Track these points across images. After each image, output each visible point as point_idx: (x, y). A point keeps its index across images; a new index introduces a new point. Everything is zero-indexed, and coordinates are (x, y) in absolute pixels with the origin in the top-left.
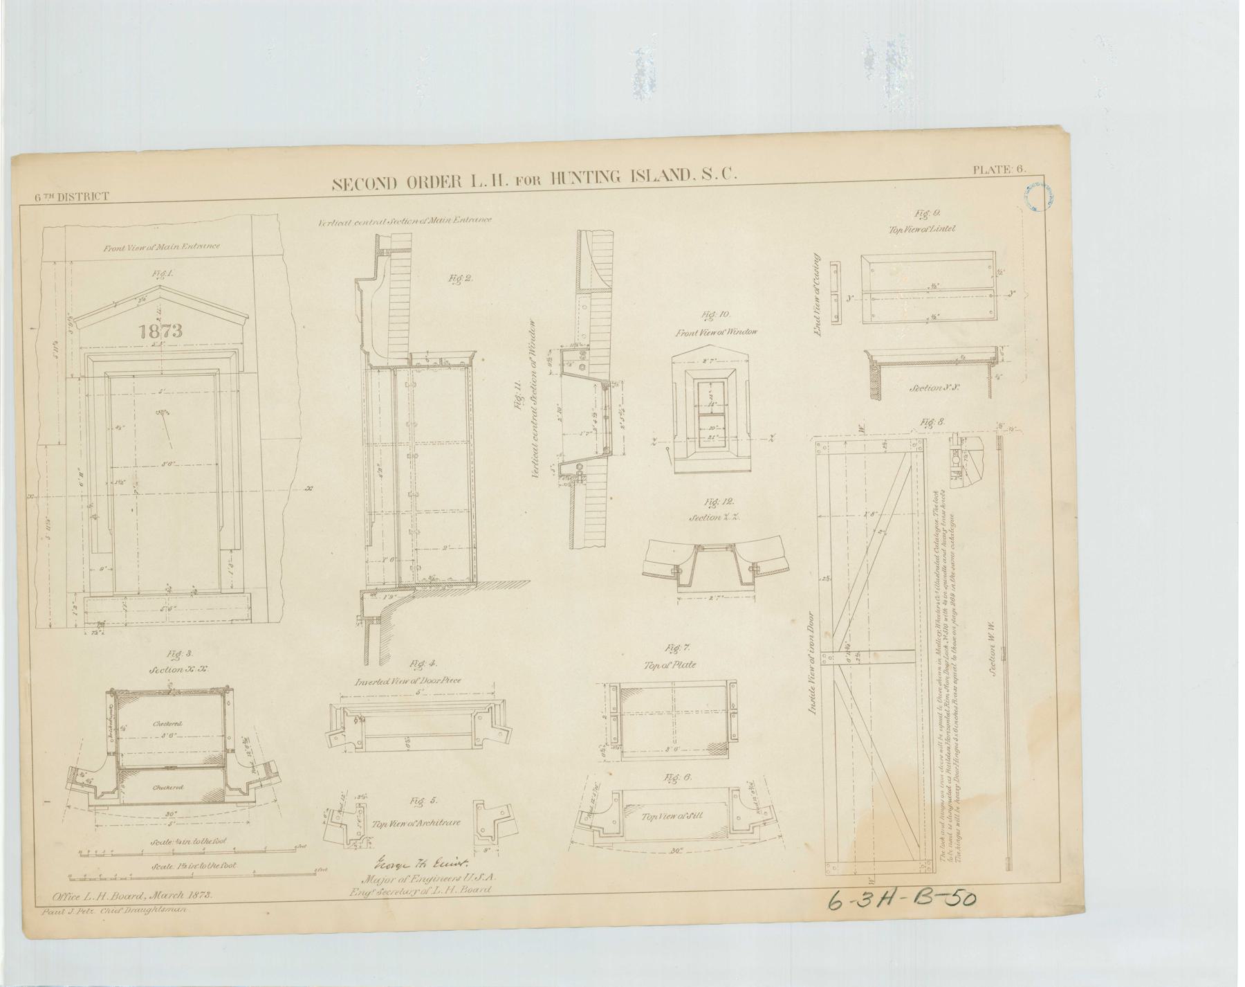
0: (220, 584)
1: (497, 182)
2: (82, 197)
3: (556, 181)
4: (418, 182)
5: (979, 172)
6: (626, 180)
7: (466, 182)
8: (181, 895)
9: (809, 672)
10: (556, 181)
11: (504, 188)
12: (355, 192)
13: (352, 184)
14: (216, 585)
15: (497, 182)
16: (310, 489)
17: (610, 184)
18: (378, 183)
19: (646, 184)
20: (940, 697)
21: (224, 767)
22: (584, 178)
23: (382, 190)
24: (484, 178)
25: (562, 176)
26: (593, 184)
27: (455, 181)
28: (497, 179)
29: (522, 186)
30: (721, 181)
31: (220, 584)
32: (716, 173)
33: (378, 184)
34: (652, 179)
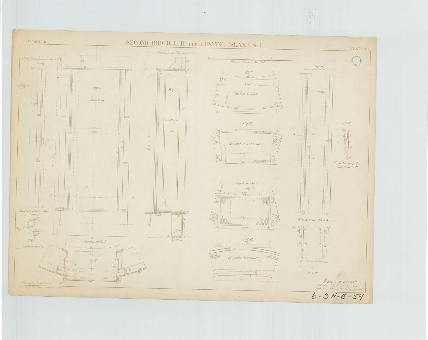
0: (72, 75)
1: (183, 44)
2: (41, 42)
4: (156, 43)
5: (352, 49)
6: (150, 44)
7: (172, 44)
9: (246, 182)
11: (249, 47)
13: (133, 42)
15: (183, 44)
16: (96, 88)
17: (221, 47)
18: (142, 42)
19: (129, 45)
21: (122, 209)
22: (212, 44)
23: (143, 45)
24: (178, 43)
26: (215, 46)
28: (182, 43)
30: (259, 47)
31: (72, 75)
32: (258, 45)
33: (142, 43)
34: (176, 44)
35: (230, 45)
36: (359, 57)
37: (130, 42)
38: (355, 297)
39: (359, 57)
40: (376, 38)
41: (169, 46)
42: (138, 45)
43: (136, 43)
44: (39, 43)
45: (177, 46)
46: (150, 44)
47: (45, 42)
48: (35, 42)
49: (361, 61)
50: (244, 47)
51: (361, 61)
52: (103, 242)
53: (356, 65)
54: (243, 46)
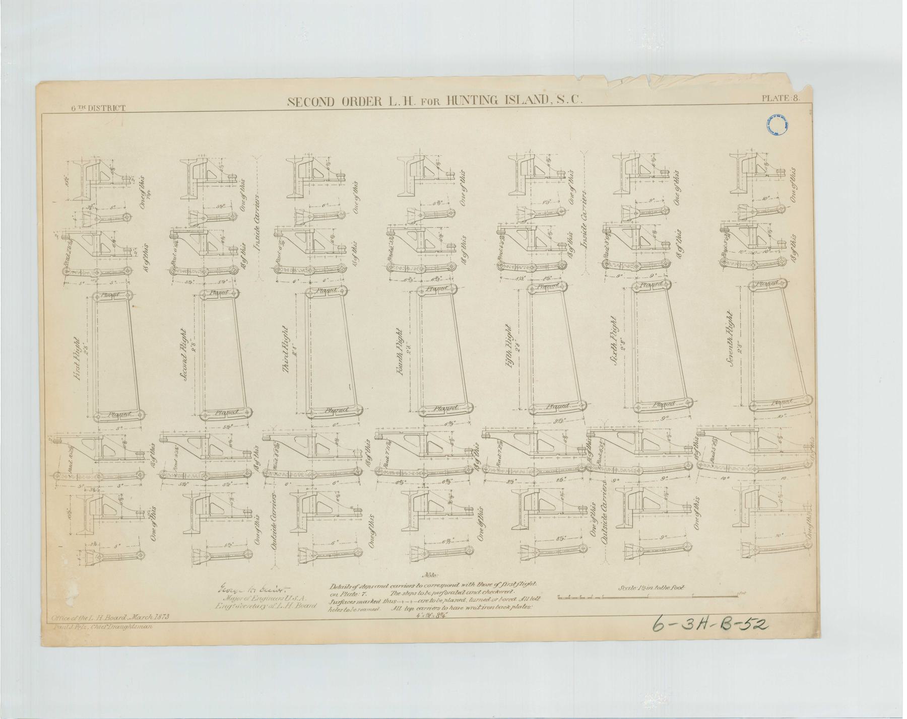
1: (408, 103)
3: (451, 102)
4: (350, 101)
6: (339, 104)
7: (385, 103)
8: (150, 617)
10: (451, 102)
13: (302, 102)
15: (408, 103)
17: (490, 105)
18: (320, 101)
22: (471, 100)
23: (324, 107)
24: (399, 100)
25: (455, 99)
27: (378, 101)
28: (408, 101)
29: (426, 105)
32: (567, 99)
33: (321, 103)
35: (509, 100)
39: (769, 121)
45: (397, 107)
46: (339, 104)
47: (115, 107)
53: (776, 134)
54: (485, 102)
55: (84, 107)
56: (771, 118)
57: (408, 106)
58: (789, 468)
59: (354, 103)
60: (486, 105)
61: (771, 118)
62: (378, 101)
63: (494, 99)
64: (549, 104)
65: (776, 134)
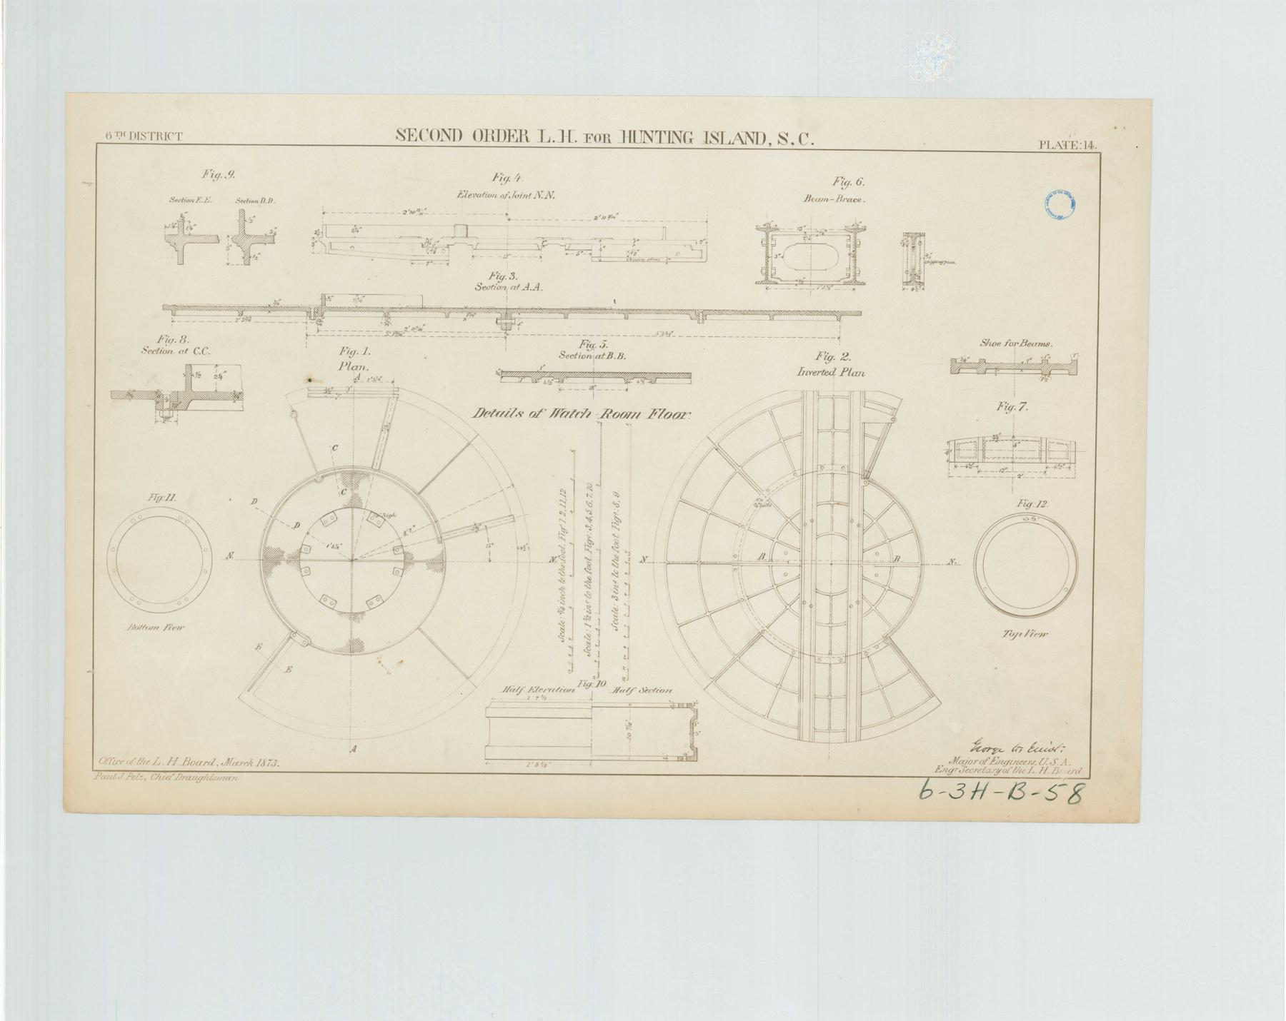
1: (566, 139)
2: (155, 136)
3: (627, 139)
4: (484, 134)
5: (1045, 146)
6: (467, 140)
12: (419, 142)
13: (416, 135)
14: (834, 602)
15: (566, 139)
17: (683, 145)
20: (587, 618)
22: (656, 137)
23: (447, 142)
27: (524, 135)
32: (793, 138)
34: (545, 139)
35: (710, 138)
36: (1067, 193)
37: (406, 135)
38: (1052, 796)
39: (1067, 193)
40: (1149, 102)
41: (525, 144)
42: (430, 142)
43: (426, 135)
44: (148, 141)
45: (551, 144)
46: (467, 140)
47: (167, 136)
48: (137, 135)
49: (1073, 204)
50: (750, 144)
51: (1073, 204)
52: (616, 500)
53: (1060, 218)
54: (445, 137)
55: (123, 134)
56: (1060, 192)
57: (566, 143)
58: (601, 374)
59: (490, 138)
60: (678, 144)
61: (1060, 192)
62: (524, 135)
63: (688, 136)
64: (766, 145)
65: (1060, 218)
